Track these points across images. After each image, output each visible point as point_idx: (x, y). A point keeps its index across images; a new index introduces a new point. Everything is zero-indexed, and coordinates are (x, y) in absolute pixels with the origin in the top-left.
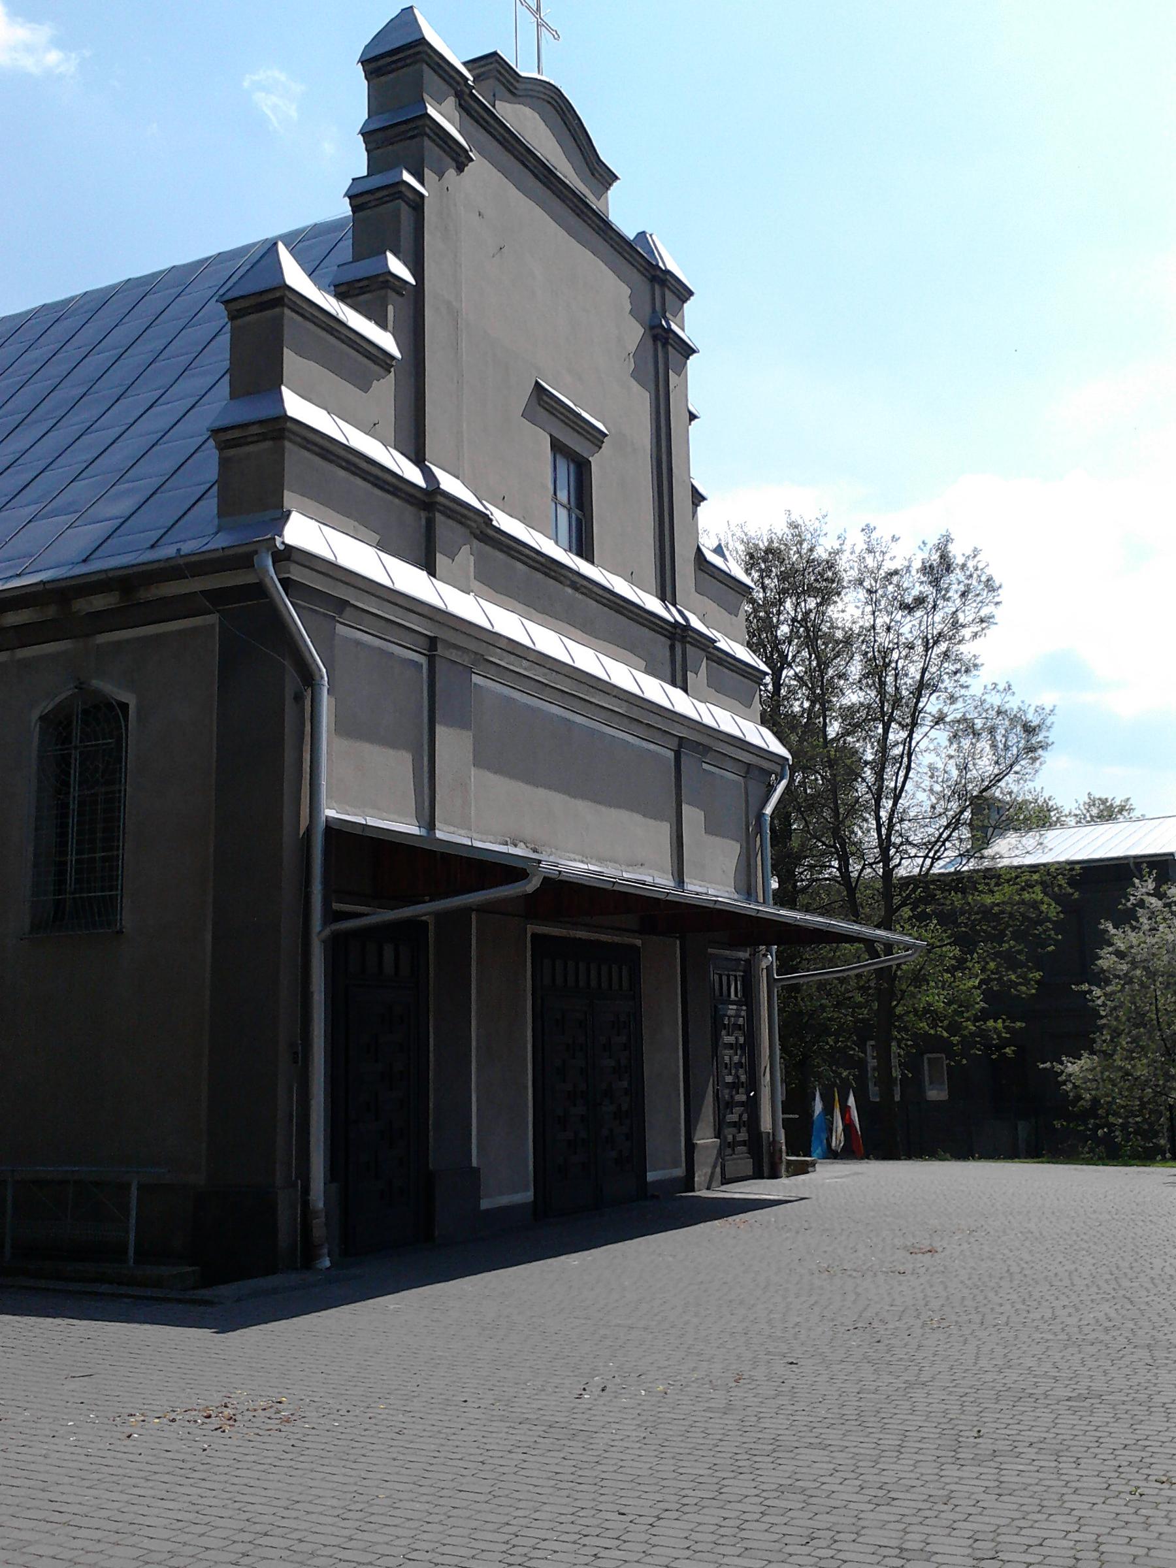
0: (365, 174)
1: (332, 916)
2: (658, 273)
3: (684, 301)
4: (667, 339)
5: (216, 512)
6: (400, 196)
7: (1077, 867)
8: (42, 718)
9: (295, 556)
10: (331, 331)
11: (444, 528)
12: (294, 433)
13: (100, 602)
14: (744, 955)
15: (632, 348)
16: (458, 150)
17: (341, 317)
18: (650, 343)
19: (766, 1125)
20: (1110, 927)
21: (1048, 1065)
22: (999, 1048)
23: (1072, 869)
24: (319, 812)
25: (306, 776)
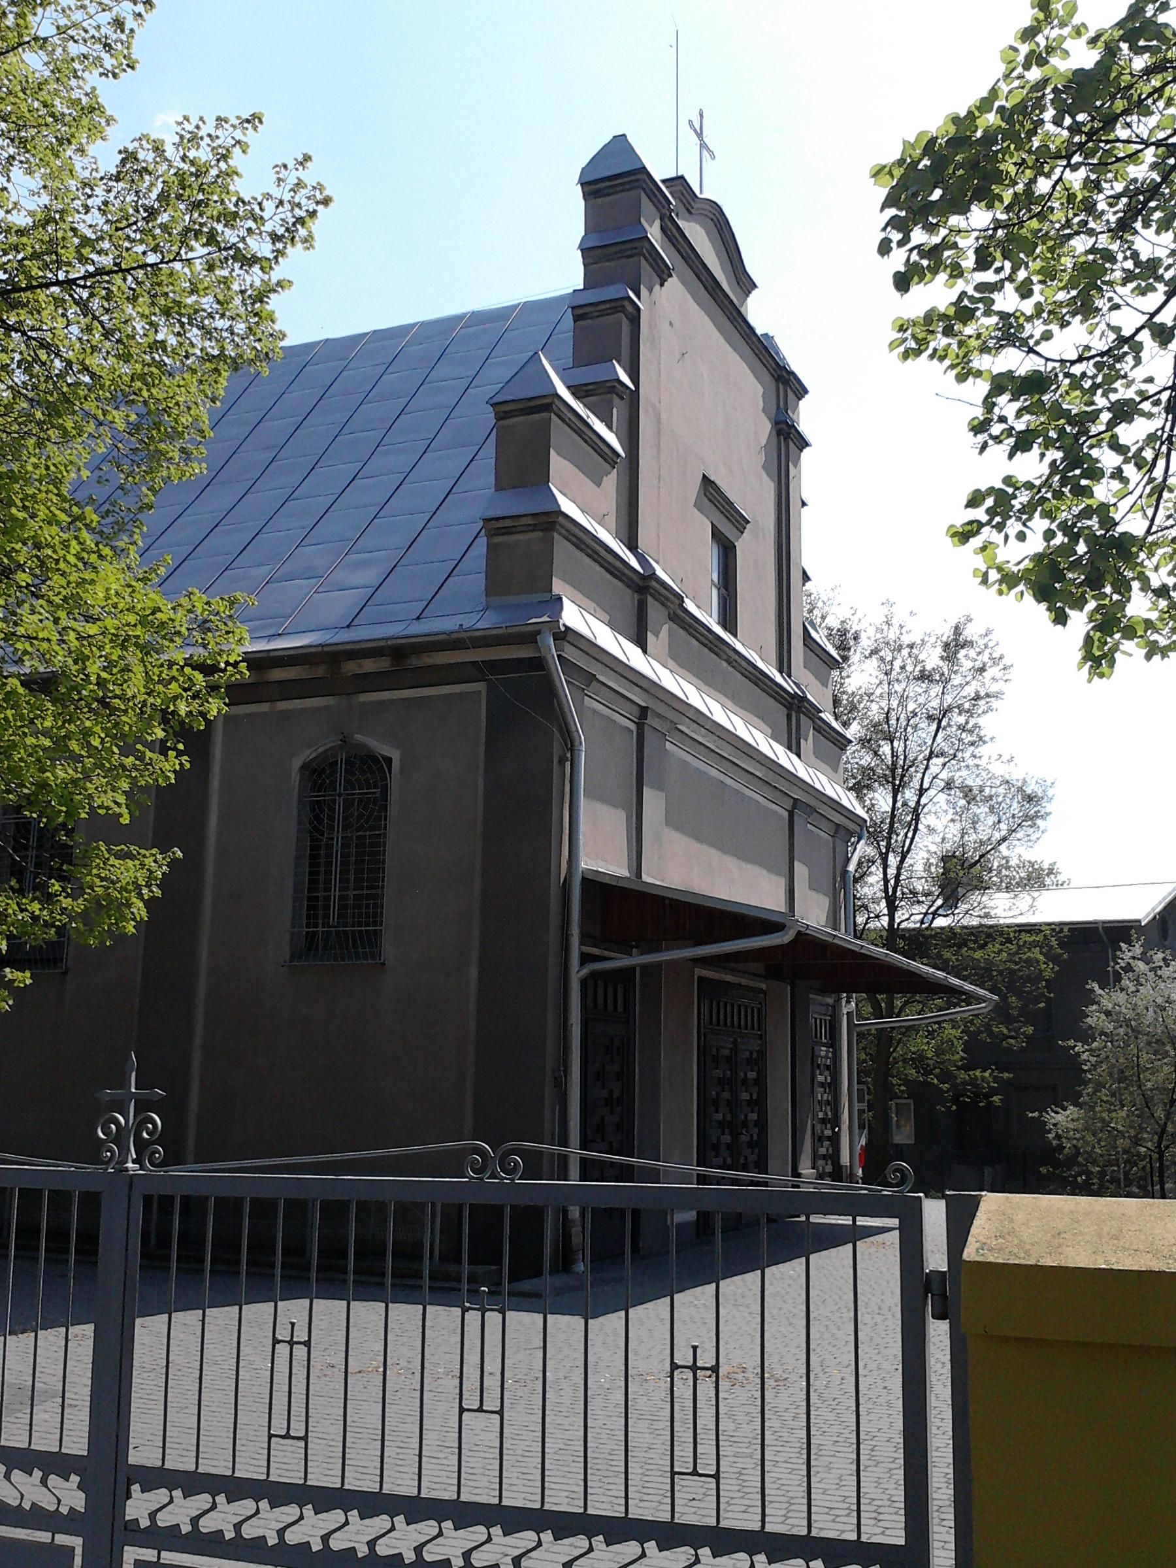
0: (582, 287)
1: (585, 959)
2: (784, 373)
3: (800, 399)
4: (789, 434)
5: (483, 588)
6: (623, 310)
7: (1066, 929)
8: (304, 767)
9: (570, 637)
10: (580, 434)
11: (654, 610)
12: (563, 527)
13: (369, 666)
14: (830, 1001)
15: (763, 442)
16: (662, 266)
17: (589, 421)
18: (774, 433)
19: (845, 1159)
20: (1096, 986)
21: (1036, 1114)
22: (987, 1096)
23: (1061, 931)
24: (578, 865)
25: (566, 831)
